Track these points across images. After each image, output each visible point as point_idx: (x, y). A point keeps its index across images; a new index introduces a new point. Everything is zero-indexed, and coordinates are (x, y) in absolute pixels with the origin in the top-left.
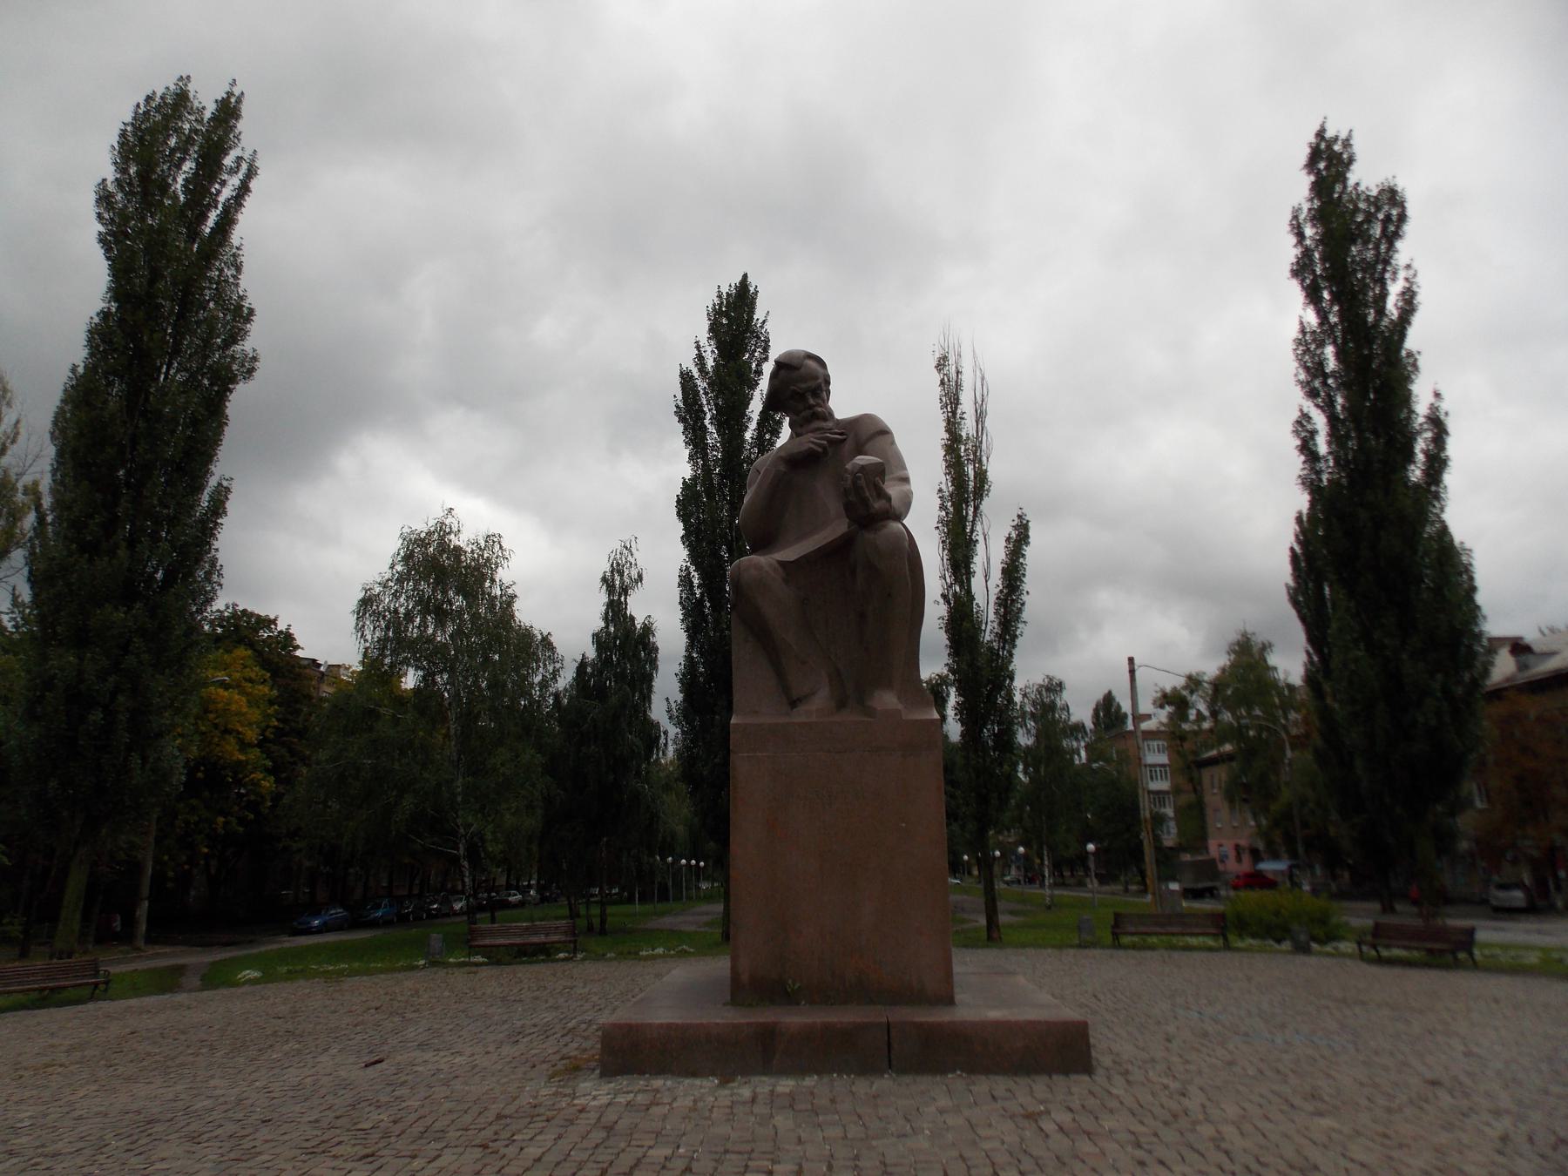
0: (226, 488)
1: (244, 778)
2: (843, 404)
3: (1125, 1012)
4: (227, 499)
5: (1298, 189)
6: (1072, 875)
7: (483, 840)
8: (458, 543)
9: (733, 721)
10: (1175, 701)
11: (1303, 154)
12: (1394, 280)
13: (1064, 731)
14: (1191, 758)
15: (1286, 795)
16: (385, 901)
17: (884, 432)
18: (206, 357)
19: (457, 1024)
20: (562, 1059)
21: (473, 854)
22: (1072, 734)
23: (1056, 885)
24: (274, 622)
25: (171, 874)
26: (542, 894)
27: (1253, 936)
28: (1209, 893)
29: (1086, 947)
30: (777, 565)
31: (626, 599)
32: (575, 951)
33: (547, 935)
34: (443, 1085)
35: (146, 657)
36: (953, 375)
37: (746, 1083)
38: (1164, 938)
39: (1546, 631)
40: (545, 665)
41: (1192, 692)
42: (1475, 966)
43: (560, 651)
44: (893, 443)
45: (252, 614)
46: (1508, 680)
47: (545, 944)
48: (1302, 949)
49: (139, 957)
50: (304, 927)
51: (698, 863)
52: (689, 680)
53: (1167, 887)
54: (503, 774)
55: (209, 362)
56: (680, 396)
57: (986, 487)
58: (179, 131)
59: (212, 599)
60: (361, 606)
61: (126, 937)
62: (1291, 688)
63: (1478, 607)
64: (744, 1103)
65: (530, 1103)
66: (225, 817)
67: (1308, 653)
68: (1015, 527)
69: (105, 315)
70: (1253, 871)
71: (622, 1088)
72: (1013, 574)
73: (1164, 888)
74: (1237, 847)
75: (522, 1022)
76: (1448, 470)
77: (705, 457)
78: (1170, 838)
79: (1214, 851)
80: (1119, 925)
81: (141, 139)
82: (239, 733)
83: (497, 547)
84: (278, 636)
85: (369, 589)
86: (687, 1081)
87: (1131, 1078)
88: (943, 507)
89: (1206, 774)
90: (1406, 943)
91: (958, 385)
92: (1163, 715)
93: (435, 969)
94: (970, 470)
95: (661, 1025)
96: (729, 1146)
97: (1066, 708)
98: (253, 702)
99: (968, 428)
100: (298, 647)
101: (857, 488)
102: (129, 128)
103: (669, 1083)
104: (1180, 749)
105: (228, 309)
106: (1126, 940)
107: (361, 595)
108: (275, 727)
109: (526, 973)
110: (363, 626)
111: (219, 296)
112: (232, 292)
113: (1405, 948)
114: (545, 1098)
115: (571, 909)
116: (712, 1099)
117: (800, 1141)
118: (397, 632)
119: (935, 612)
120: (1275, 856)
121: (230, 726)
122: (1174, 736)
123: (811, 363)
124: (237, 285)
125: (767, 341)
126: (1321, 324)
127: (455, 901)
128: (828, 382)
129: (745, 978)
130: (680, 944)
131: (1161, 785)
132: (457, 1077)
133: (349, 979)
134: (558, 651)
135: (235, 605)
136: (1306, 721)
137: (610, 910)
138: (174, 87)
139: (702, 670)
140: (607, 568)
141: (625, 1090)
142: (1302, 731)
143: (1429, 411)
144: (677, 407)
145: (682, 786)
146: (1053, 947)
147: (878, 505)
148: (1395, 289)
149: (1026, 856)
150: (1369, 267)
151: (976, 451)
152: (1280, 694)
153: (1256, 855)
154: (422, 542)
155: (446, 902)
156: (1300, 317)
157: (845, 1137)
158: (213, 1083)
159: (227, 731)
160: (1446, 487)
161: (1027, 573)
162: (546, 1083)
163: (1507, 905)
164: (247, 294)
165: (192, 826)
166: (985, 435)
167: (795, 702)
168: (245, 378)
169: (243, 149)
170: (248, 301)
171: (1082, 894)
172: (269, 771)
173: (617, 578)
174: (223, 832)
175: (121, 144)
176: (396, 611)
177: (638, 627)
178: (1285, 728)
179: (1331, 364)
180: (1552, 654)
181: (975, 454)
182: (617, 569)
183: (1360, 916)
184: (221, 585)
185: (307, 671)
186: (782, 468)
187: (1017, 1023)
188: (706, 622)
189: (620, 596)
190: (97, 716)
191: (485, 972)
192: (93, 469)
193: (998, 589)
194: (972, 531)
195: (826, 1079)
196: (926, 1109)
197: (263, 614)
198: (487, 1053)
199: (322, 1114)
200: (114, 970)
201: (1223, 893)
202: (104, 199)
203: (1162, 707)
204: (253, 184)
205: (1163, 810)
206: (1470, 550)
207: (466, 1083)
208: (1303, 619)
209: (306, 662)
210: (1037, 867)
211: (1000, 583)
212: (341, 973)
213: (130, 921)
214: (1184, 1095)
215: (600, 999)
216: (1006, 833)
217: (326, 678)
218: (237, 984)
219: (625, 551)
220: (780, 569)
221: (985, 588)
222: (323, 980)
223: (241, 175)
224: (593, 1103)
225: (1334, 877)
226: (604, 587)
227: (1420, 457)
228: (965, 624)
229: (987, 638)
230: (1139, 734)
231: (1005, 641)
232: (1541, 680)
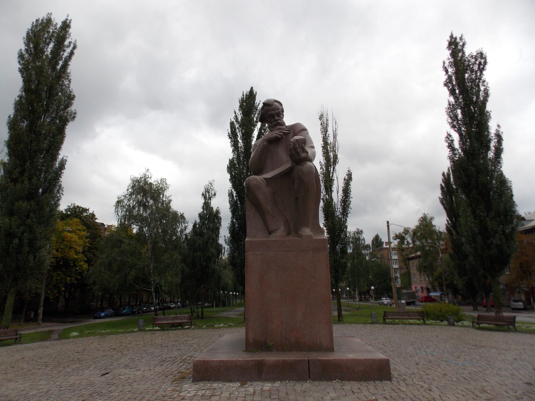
0: (65, 160)
1: (77, 264)
2: (288, 120)
3: (397, 351)
4: (66, 164)
5: (446, 55)
7: (161, 286)
8: (151, 182)
9: (246, 240)
10: (401, 237)
13: (363, 247)
14: (406, 257)
15: (439, 270)
16: (127, 307)
18: (58, 113)
19: (141, 357)
20: (179, 373)
21: (157, 290)
22: (366, 249)
23: (360, 300)
24: (88, 210)
25: (51, 298)
27: (432, 319)
28: (413, 303)
29: (374, 324)
30: (264, 180)
31: (210, 201)
32: (191, 325)
33: (181, 320)
34: (129, 385)
35: (35, 220)
37: (251, 385)
38: (401, 320)
39: (527, 214)
40: (182, 224)
41: (406, 234)
42: (516, 331)
44: (308, 134)
45: (80, 207)
47: (181, 323)
48: (451, 324)
49: (39, 327)
50: (99, 316)
51: (236, 293)
52: (232, 230)
53: (401, 302)
54: (167, 262)
55: (59, 115)
56: (230, 130)
57: (337, 160)
58: (48, 32)
59: (60, 199)
60: (117, 204)
61: (35, 320)
62: (440, 233)
63: (514, 202)
65: (162, 394)
66: (70, 278)
67: (447, 221)
68: (347, 175)
69: (21, 97)
70: (427, 296)
71: (200, 388)
72: (346, 191)
73: (399, 302)
74: (422, 287)
75: (166, 356)
76: (503, 153)
77: (238, 151)
78: (399, 284)
79: (414, 289)
80: (385, 315)
81: (35, 35)
82: (75, 248)
84: (90, 215)
85: (120, 198)
86: (227, 384)
87: (407, 382)
89: (411, 262)
91: (327, 125)
93: (140, 332)
94: (331, 154)
95: (217, 361)
97: (364, 239)
98: (80, 238)
99: (331, 140)
100: (96, 219)
101: (295, 149)
102: (30, 31)
103: (220, 385)
104: (402, 254)
105: (66, 96)
106: (387, 321)
107: (117, 200)
108: (88, 246)
109: (172, 334)
110: (118, 211)
111: (62, 90)
112: (67, 90)
113: (489, 324)
114: (169, 392)
115: (191, 310)
116: (237, 393)
118: (130, 212)
120: (435, 291)
121: (72, 246)
122: (400, 249)
123: (276, 104)
124: (69, 87)
126: (456, 102)
127: (152, 307)
128: (283, 111)
129: (251, 341)
130: (231, 323)
131: (396, 266)
132: (136, 381)
133: (109, 336)
134: (186, 219)
135: (74, 204)
136: (446, 244)
137: (205, 310)
138: (46, 17)
139: (237, 226)
140: (204, 191)
141: (202, 388)
142: (445, 248)
143: (496, 132)
144: (229, 133)
145: (230, 267)
146: (362, 323)
147: (303, 155)
149: (349, 291)
150: (473, 81)
151: (334, 147)
152: (437, 235)
153: (428, 290)
154: (138, 181)
155: (149, 307)
156: (448, 100)
158: (41, 382)
159: (71, 248)
160: (502, 159)
161: (352, 191)
162: (171, 384)
164: (73, 90)
165: (59, 281)
166: (337, 143)
167: (270, 232)
168: (72, 120)
170: (73, 93)
171: (369, 304)
172: (86, 262)
173: (207, 194)
174: (70, 283)
175: (27, 36)
176: (129, 205)
177: (214, 211)
179: (460, 116)
181: (333, 149)
182: (207, 191)
183: (468, 311)
184: (63, 194)
185: (100, 227)
186: (265, 143)
187: (360, 360)
188: (238, 208)
189: (208, 200)
190: (16, 241)
191: (158, 333)
192: (16, 152)
193: (342, 196)
194: (332, 176)
195: (284, 383)
196: (325, 398)
197: (84, 207)
198: (150, 370)
199: (78, 399)
200: (22, 332)
201: (417, 303)
202: (21, 56)
203: (396, 239)
204: (75, 51)
206: (511, 181)
207: (138, 384)
208: (445, 209)
209: (99, 224)
210: (352, 294)
212: (107, 334)
213: (36, 314)
214: (430, 390)
215: (197, 346)
216: (342, 283)
218: (70, 338)
220: (265, 181)
222: (100, 336)
223: (71, 48)
224: (189, 395)
225: (456, 298)
226: (203, 197)
227: (493, 148)
228: (330, 209)
229: (338, 214)
230: (391, 248)
231: (344, 215)
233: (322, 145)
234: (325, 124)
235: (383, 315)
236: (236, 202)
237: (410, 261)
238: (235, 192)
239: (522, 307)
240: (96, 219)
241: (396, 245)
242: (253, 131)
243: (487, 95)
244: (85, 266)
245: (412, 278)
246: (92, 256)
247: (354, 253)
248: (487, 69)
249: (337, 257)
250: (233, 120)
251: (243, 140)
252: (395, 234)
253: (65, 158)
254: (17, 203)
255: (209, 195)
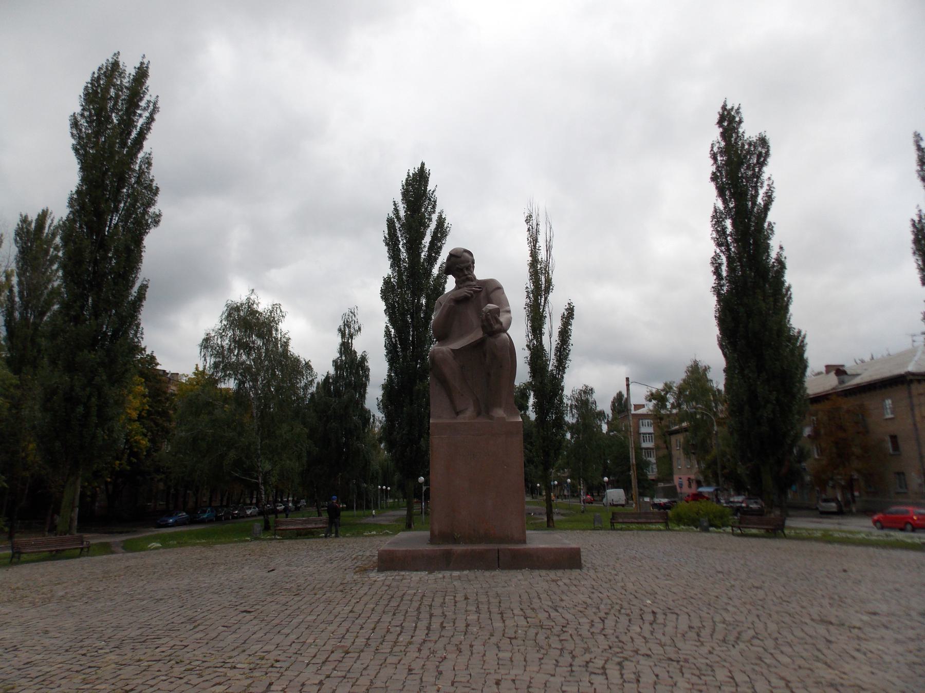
2: (480, 273)
6: (598, 495)
11: (716, 117)
12: (762, 187)
14: (665, 430)
15: (715, 451)
17: (499, 288)
25: (89, 493)
26: (296, 506)
31: (352, 341)
33: (316, 524)
36: (535, 226)
39: (858, 362)
42: (786, 537)
43: (315, 370)
44: (503, 293)
46: (834, 389)
48: (706, 530)
50: (164, 523)
52: (389, 388)
56: (387, 232)
57: (551, 287)
64: (440, 578)
72: (564, 334)
74: (689, 479)
77: (399, 267)
79: (676, 481)
83: (279, 311)
86: (415, 573)
88: (528, 297)
89: (674, 439)
90: (759, 527)
91: (537, 231)
92: (651, 405)
96: (437, 590)
99: (542, 255)
100: (157, 364)
101: (488, 320)
103: (407, 573)
104: (660, 424)
106: (619, 526)
108: (148, 410)
117: (464, 589)
119: (522, 356)
120: (709, 485)
122: (657, 417)
123: (466, 254)
124: (149, 173)
125: (435, 202)
126: (725, 208)
129: (437, 533)
134: (314, 370)
140: (341, 323)
144: (385, 237)
147: (497, 327)
148: (762, 192)
150: (749, 179)
155: (243, 510)
157: (482, 587)
163: (826, 510)
166: (551, 260)
169: (150, 96)
175: (86, 95)
177: (359, 357)
178: (715, 414)
180: (858, 375)
181: (545, 270)
182: (347, 324)
184: (142, 338)
186: (452, 304)
189: (348, 340)
190: (80, 409)
194: (543, 311)
202: (75, 124)
203: (650, 401)
204: (156, 117)
205: (649, 459)
211: (557, 339)
216: (562, 471)
217: (171, 381)
219: (351, 314)
220: (452, 353)
221: (550, 342)
228: (539, 361)
231: (560, 370)
232: (864, 386)
233: (529, 262)
234: (535, 230)
235: (611, 517)
236: (395, 346)
237: (672, 436)
238: (393, 330)
239: (835, 510)
240: (157, 364)
241: (651, 411)
242: (423, 236)
243: (769, 199)
244: (144, 443)
245: (675, 464)
246: (154, 426)
247: (578, 424)
248: (769, 164)
249: (548, 433)
250: (391, 215)
251: (408, 251)
252: (651, 391)
253: (145, 283)
254: (81, 354)
255: (350, 331)
